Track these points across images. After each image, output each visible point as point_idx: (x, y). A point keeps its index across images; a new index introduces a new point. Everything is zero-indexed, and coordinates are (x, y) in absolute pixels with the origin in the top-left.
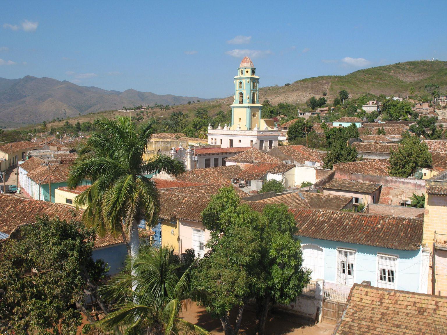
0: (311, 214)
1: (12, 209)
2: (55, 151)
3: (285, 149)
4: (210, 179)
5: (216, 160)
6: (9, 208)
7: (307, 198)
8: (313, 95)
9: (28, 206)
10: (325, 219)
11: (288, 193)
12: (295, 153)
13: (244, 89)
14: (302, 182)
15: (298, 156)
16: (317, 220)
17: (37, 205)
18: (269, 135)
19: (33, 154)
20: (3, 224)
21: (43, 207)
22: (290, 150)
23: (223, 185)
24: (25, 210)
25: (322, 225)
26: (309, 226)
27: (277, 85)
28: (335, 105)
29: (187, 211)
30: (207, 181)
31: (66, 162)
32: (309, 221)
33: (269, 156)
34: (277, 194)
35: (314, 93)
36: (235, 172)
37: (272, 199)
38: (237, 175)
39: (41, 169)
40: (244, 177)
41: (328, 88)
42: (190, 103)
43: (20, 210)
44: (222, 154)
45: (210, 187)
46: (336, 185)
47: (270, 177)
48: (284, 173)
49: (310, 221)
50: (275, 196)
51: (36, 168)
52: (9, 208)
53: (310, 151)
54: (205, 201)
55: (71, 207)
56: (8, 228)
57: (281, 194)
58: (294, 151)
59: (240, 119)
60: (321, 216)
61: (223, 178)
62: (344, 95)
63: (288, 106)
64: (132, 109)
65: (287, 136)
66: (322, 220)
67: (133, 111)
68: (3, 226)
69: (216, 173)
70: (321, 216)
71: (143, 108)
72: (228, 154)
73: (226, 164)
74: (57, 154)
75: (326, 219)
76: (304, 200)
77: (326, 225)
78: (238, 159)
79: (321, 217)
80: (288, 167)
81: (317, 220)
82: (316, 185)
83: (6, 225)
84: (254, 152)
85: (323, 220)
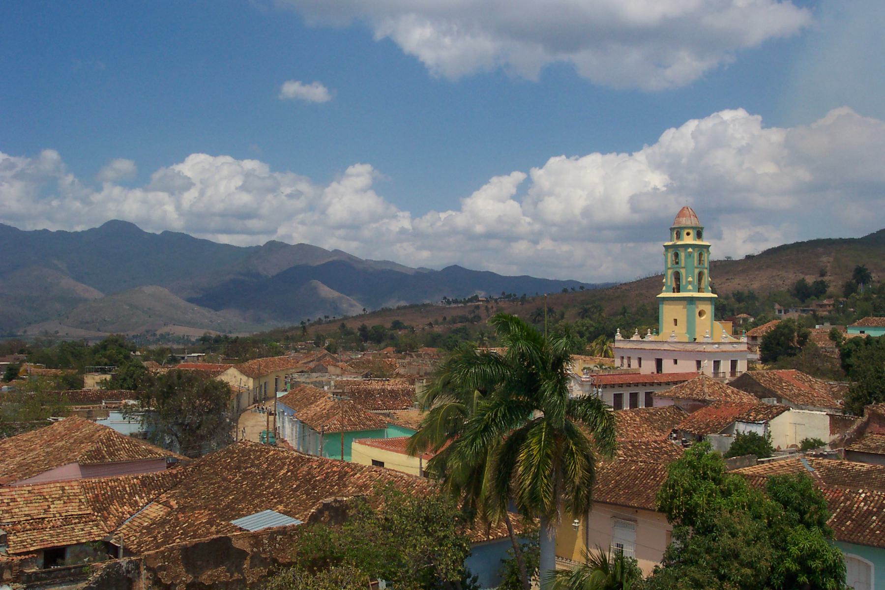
0: (843, 498)
1: (289, 474)
2: (338, 376)
3: (763, 376)
4: (627, 431)
5: (634, 397)
6: (283, 472)
7: (818, 469)
8: (801, 276)
9: (319, 470)
10: (871, 508)
11: (781, 459)
12: (784, 384)
13: (683, 265)
14: (803, 438)
15: (790, 391)
16: (855, 508)
17: (335, 469)
18: (731, 350)
19: (299, 380)
20: (275, 500)
21: (347, 473)
22: (774, 379)
23: (655, 442)
24: (314, 477)
25: (866, 518)
26: (841, 520)
27: (730, 258)
28: (846, 295)
29: (603, 487)
30: (622, 434)
31: (361, 396)
32: (838, 510)
33: (735, 390)
34: (762, 459)
35: (802, 273)
36: (673, 418)
37: (753, 470)
38: (678, 424)
39: (321, 406)
40: (690, 428)
41: (829, 262)
42: (565, 291)
43: (304, 476)
44: (644, 384)
45: (633, 445)
46: (873, 445)
47: (743, 428)
48: (769, 421)
49: (841, 511)
50: (758, 463)
51: (312, 403)
52: (283, 472)
53: (810, 381)
54: (635, 470)
55: (398, 473)
56: (285, 507)
57: (769, 461)
58: (781, 380)
59: (676, 321)
60: (862, 501)
61: (651, 429)
62: (861, 275)
63: (752, 297)
64: (461, 302)
65: (758, 352)
66: (865, 508)
67: (462, 305)
68: (276, 503)
69: (638, 420)
70: (862, 501)
71: (480, 301)
72: (640, 386)
73: (654, 403)
74: (341, 381)
75: (873, 508)
76: (812, 472)
77: (874, 518)
78: (677, 395)
79: (863, 504)
80: (775, 411)
81: (855, 508)
82: (833, 445)
83: (281, 502)
84: (707, 383)
85: (867, 509)
